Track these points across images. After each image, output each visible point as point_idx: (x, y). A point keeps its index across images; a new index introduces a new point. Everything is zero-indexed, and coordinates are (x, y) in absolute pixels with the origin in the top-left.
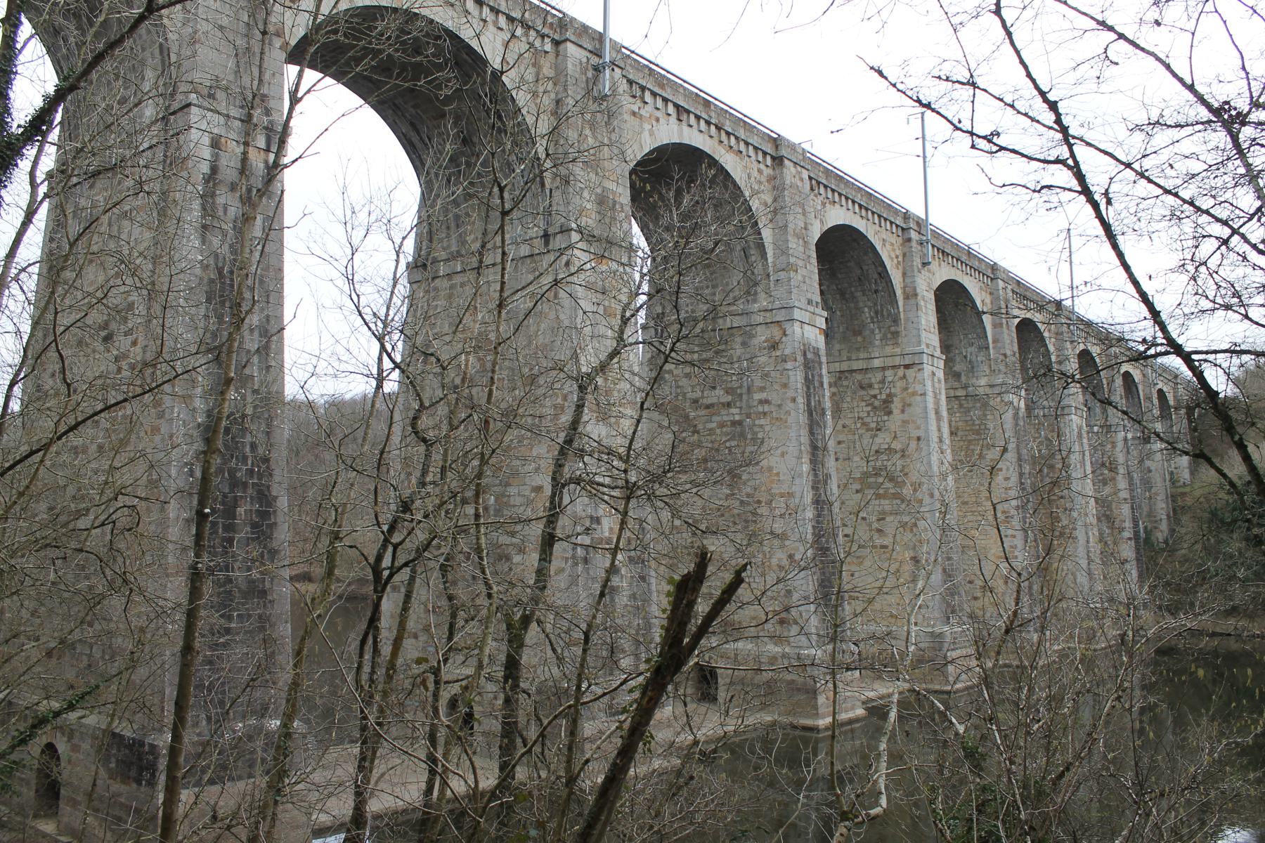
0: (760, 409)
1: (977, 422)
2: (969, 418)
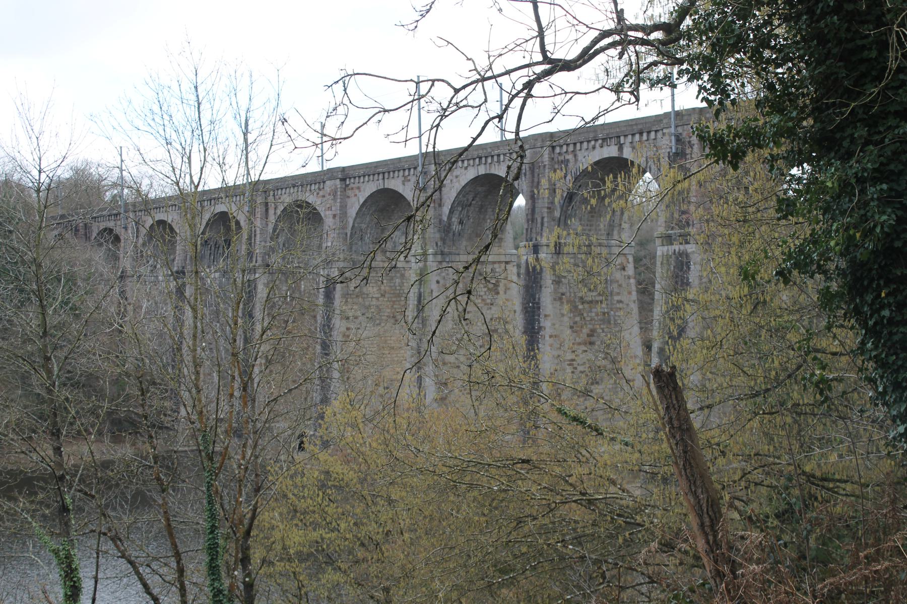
0: (618, 306)
1: (398, 288)
2: (392, 285)
